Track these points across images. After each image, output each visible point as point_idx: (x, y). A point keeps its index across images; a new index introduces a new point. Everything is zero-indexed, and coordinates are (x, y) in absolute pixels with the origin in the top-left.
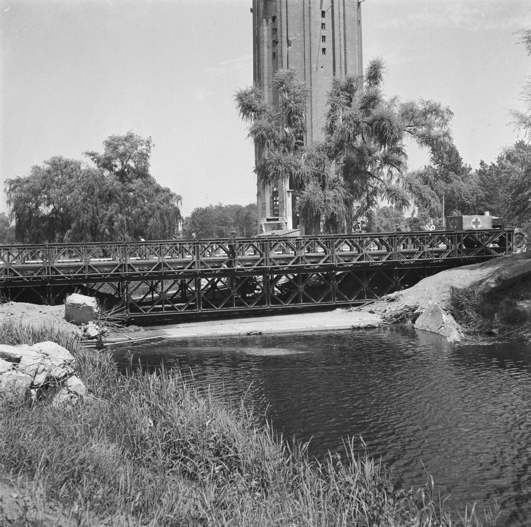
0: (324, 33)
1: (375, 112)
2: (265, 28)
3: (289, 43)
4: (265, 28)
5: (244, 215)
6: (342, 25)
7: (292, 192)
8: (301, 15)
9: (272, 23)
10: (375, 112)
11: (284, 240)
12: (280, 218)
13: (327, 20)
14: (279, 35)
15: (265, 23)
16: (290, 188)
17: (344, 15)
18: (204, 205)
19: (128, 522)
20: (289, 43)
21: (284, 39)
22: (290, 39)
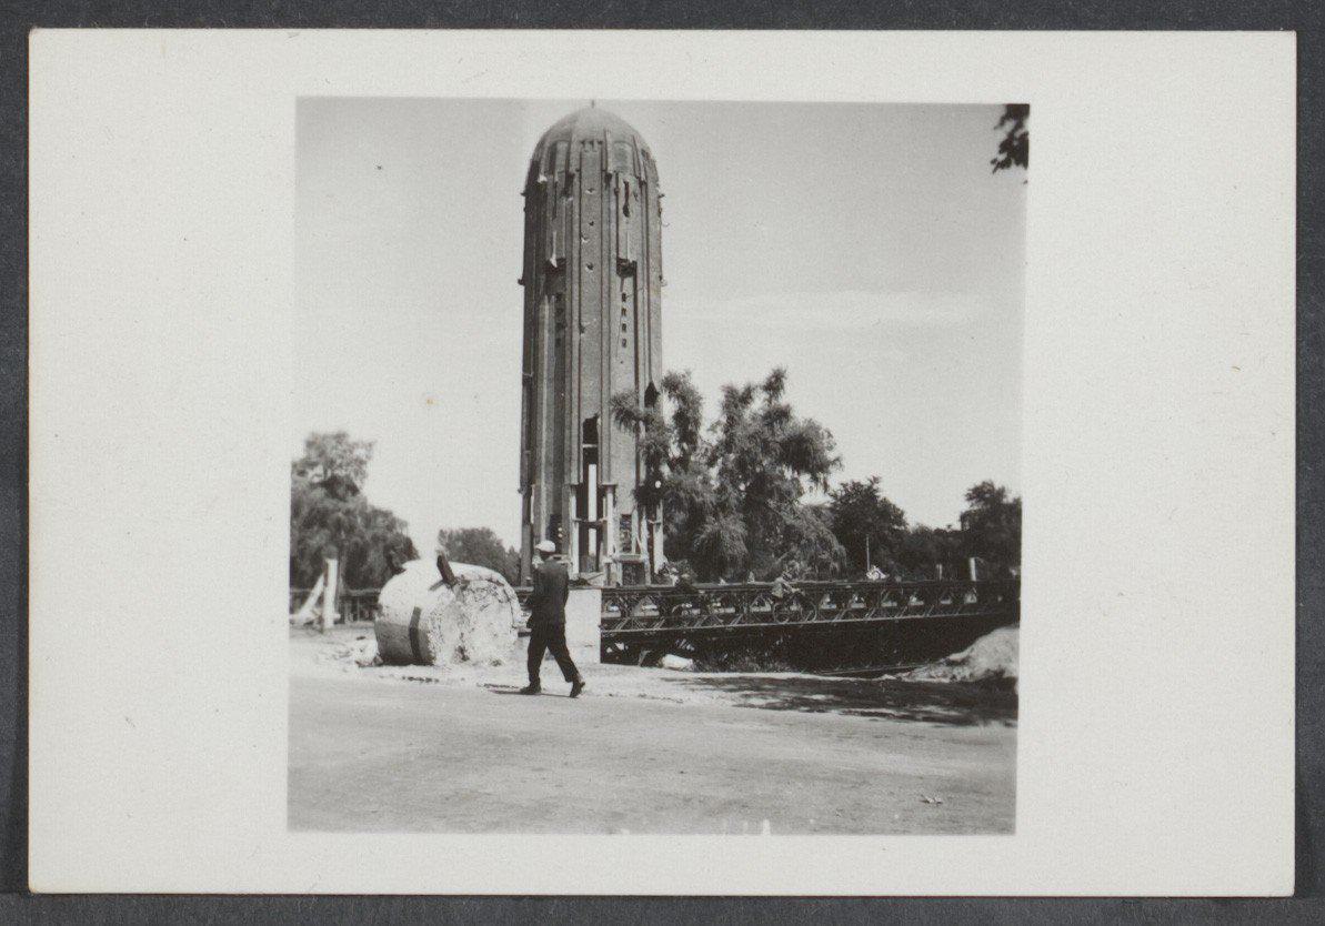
0: (624, 320)
1: (447, 535)
2: (547, 307)
3: (582, 330)
4: (547, 307)
5: (313, 552)
6: (646, 313)
7: (580, 522)
8: (598, 295)
9: (556, 302)
10: (447, 535)
11: (653, 594)
12: (563, 557)
13: (629, 305)
14: (567, 317)
15: (546, 301)
16: (577, 516)
17: (649, 300)
18: (603, 838)
19: (370, 665)
20: (582, 330)
21: (575, 324)
22: (584, 324)
